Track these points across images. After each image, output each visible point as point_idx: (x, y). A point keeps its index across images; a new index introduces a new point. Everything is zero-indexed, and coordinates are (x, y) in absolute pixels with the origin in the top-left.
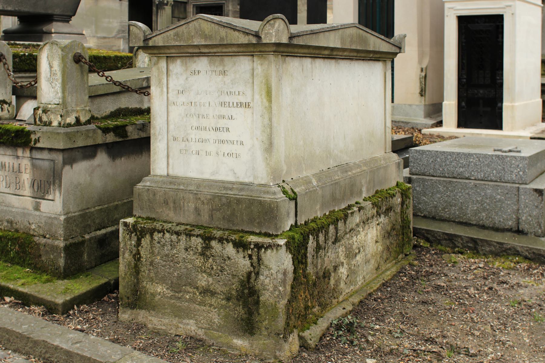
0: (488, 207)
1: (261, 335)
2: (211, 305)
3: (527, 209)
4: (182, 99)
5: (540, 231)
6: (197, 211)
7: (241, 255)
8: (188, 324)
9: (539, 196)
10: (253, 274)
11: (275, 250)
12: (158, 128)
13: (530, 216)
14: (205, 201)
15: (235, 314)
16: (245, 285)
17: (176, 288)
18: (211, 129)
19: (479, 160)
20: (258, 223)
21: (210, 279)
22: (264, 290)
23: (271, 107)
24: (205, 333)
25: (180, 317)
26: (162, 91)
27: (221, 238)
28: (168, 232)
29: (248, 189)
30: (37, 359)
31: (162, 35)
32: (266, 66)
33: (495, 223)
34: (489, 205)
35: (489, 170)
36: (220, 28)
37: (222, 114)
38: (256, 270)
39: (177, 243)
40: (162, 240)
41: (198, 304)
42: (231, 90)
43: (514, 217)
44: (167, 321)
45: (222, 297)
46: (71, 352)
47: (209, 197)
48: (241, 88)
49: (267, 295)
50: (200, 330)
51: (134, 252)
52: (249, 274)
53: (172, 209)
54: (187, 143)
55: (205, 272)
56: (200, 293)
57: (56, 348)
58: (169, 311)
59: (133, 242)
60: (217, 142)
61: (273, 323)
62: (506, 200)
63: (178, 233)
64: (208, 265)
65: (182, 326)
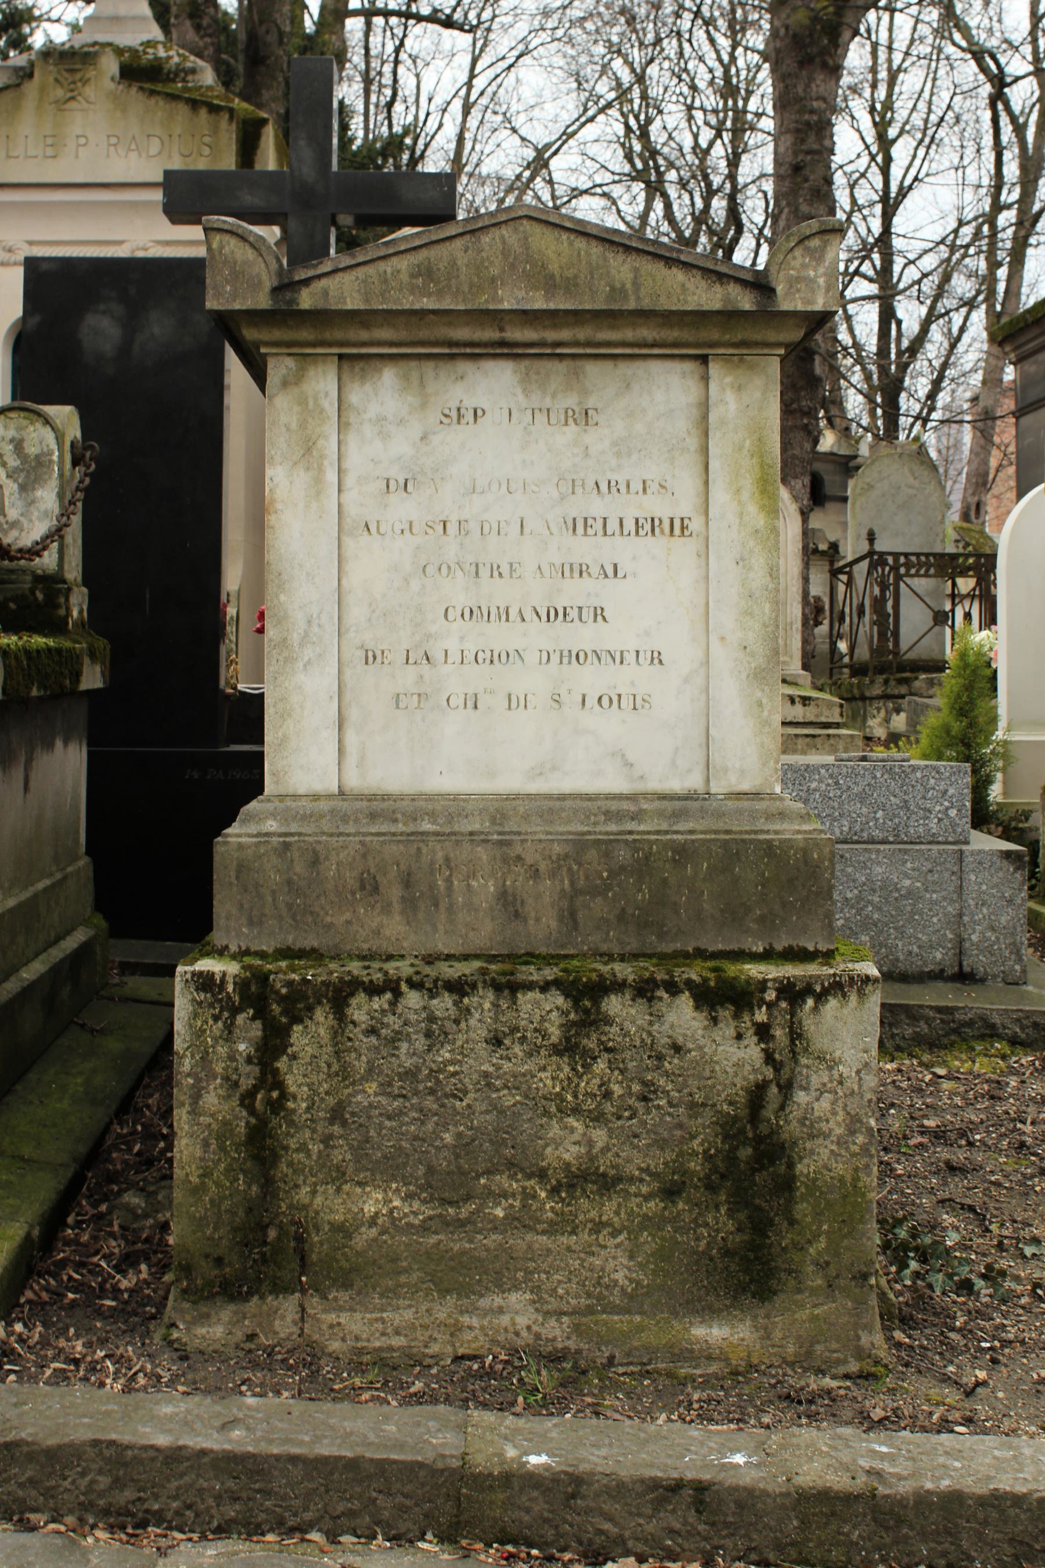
0: (876, 916)
1: (799, 1291)
2: (598, 1227)
3: (985, 911)
4: (402, 509)
5: (1017, 967)
6: (509, 904)
7: (727, 1029)
8: (501, 1310)
9: (1016, 870)
10: (774, 1089)
11: (853, 998)
12: (298, 618)
13: (992, 929)
14: (543, 867)
15: (698, 1239)
16: (742, 1131)
17: (449, 1186)
18: (529, 614)
19: (837, 783)
20: (761, 920)
21: (600, 1136)
22: (812, 1137)
23: (775, 530)
24: (576, 1328)
25: (464, 1290)
26: (318, 480)
27: (643, 981)
28: (413, 985)
29: (702, 809)
30: (70, 1520)
31: (360, 272)
32: (758, 395)
33: (897, 960)
34: (879, 909)
35: (864, 810)
36: (610, 255)
37: (576, 560)
38: (785, 1073)
39: (457, 1022)
40: (390, 1019)
41: (543, 1232)
42: (614, 477)
43: (950, 936)
44: (408, 1315)
45: (644, 1189)
46: (253, 1456)
47: (557, 849)
48: (652, 471)
49: (825, 1153)
50: (553, 1322)
51: (246, 1083)
52: (757, 1094)
53: (397, 906)
54: (425, 667)
55: (576, 1111)
56: (554, 1191)
57: (174, 1456)
58: (415, 1276)
59: (242, 1047)
60: (555, 658)
61: (845, 1242)
62: (926, 890)
63: (459, 988)
64: (589, 1084)
65: (475, 1322)
